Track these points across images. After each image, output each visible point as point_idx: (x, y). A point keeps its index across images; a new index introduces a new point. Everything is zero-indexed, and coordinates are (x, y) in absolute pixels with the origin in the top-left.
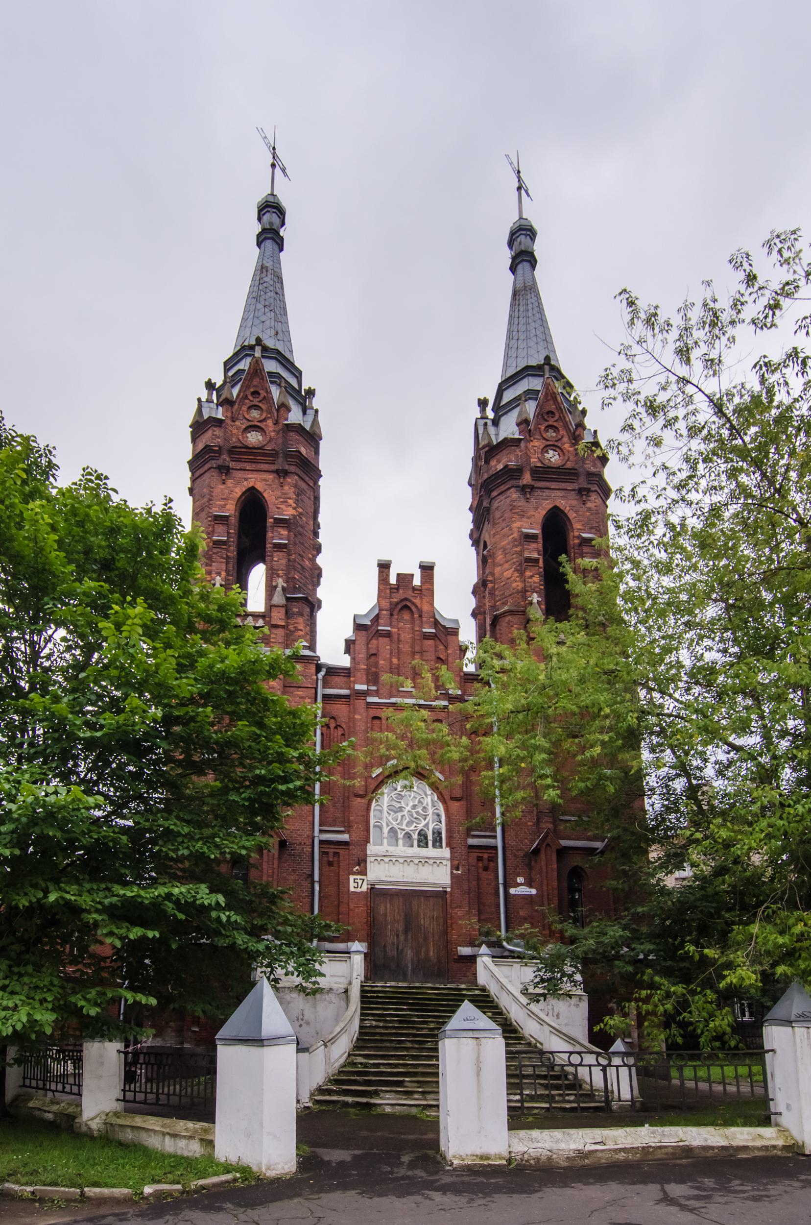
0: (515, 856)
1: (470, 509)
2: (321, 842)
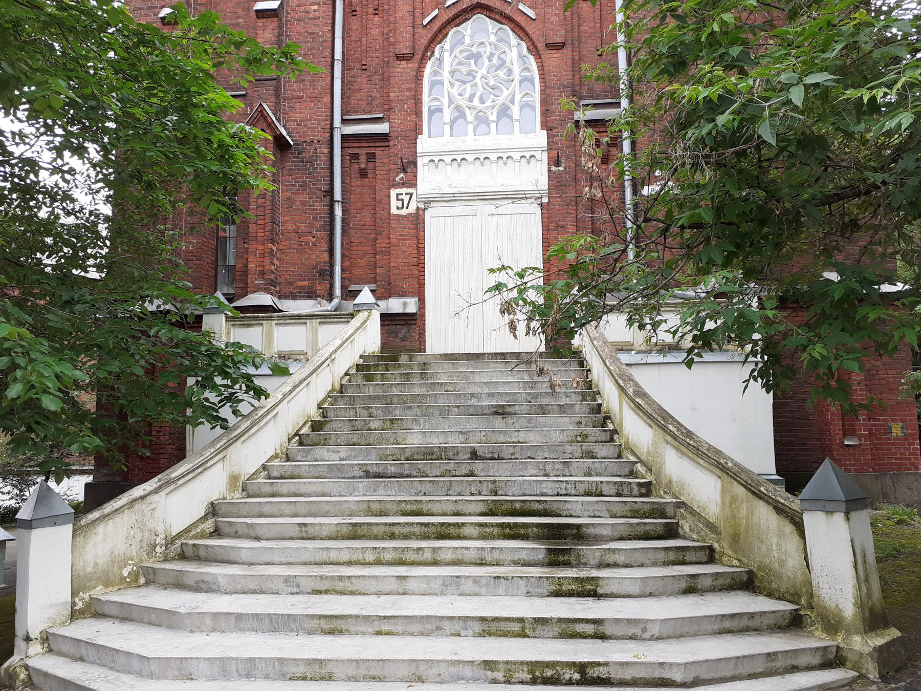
2: (344, 138)
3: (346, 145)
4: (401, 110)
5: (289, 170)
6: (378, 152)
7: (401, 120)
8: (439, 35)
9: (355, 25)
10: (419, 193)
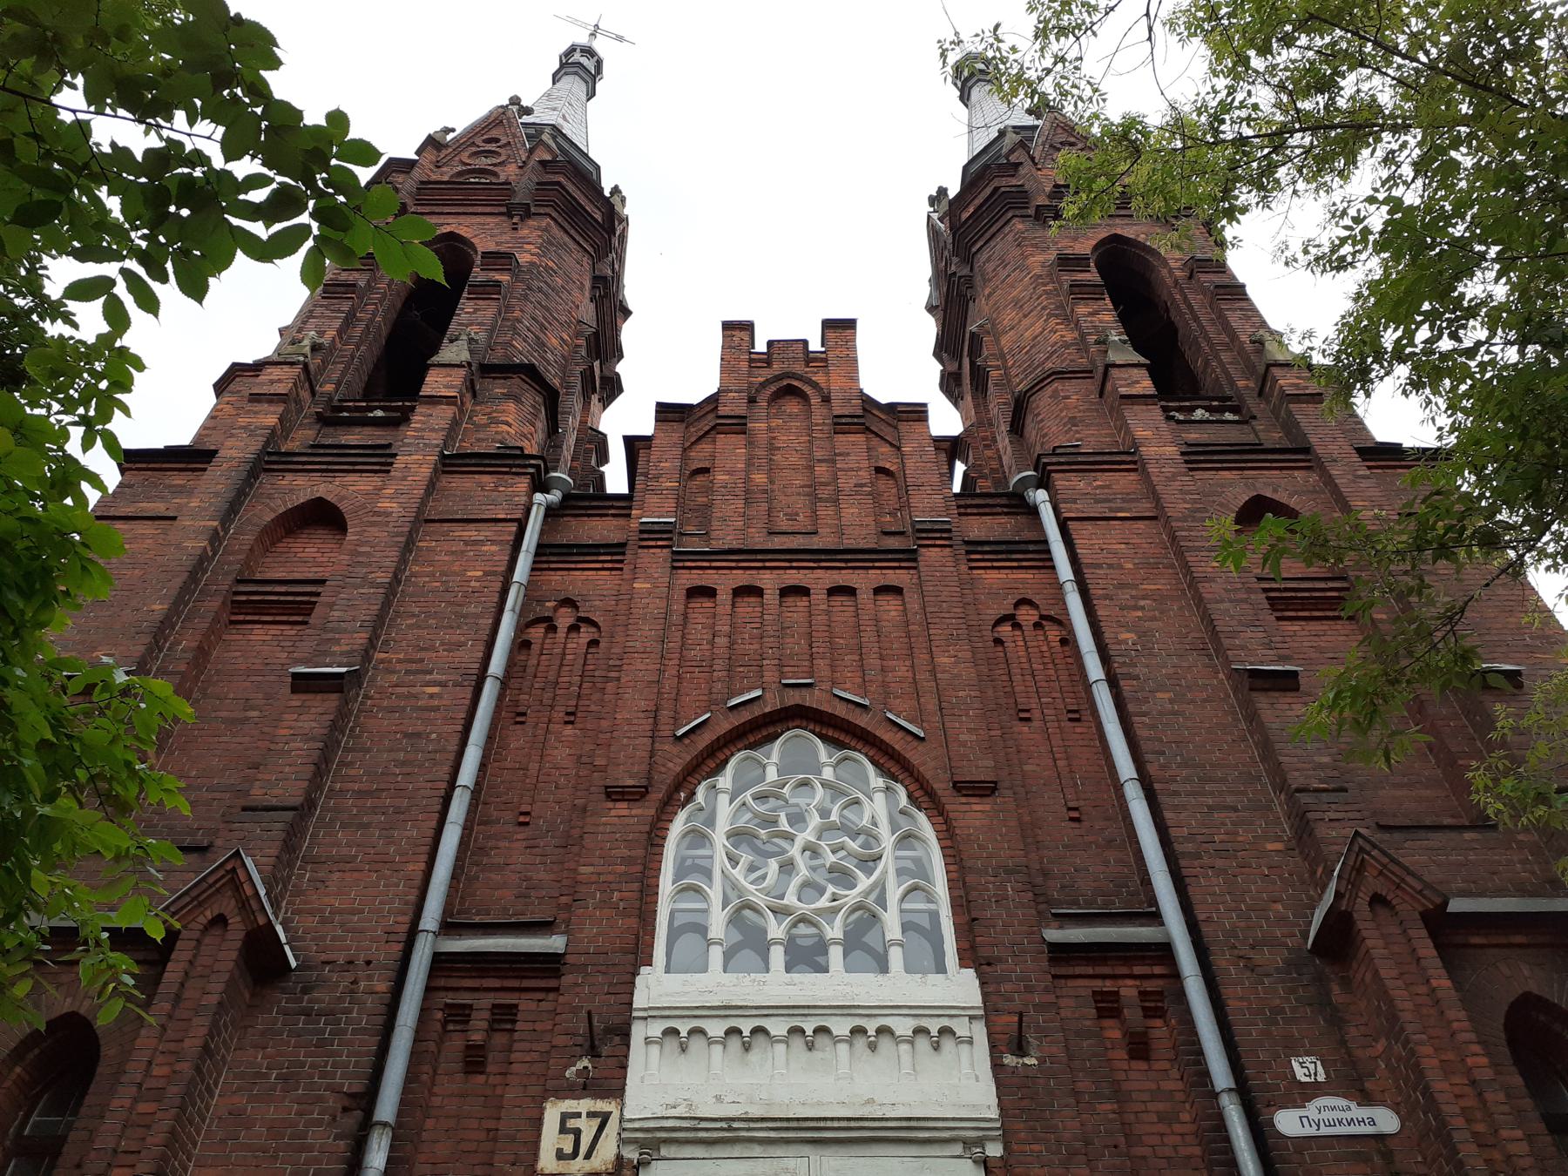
0: (1252, 967)
1: (931, 309)
3: (442, 982)
4: (604, 904)
5: (263, 1034)
6: (526, 1004)
7: (597, 928)
8: (709, 761)
9: (518, 740)
10: (627, 1115)
